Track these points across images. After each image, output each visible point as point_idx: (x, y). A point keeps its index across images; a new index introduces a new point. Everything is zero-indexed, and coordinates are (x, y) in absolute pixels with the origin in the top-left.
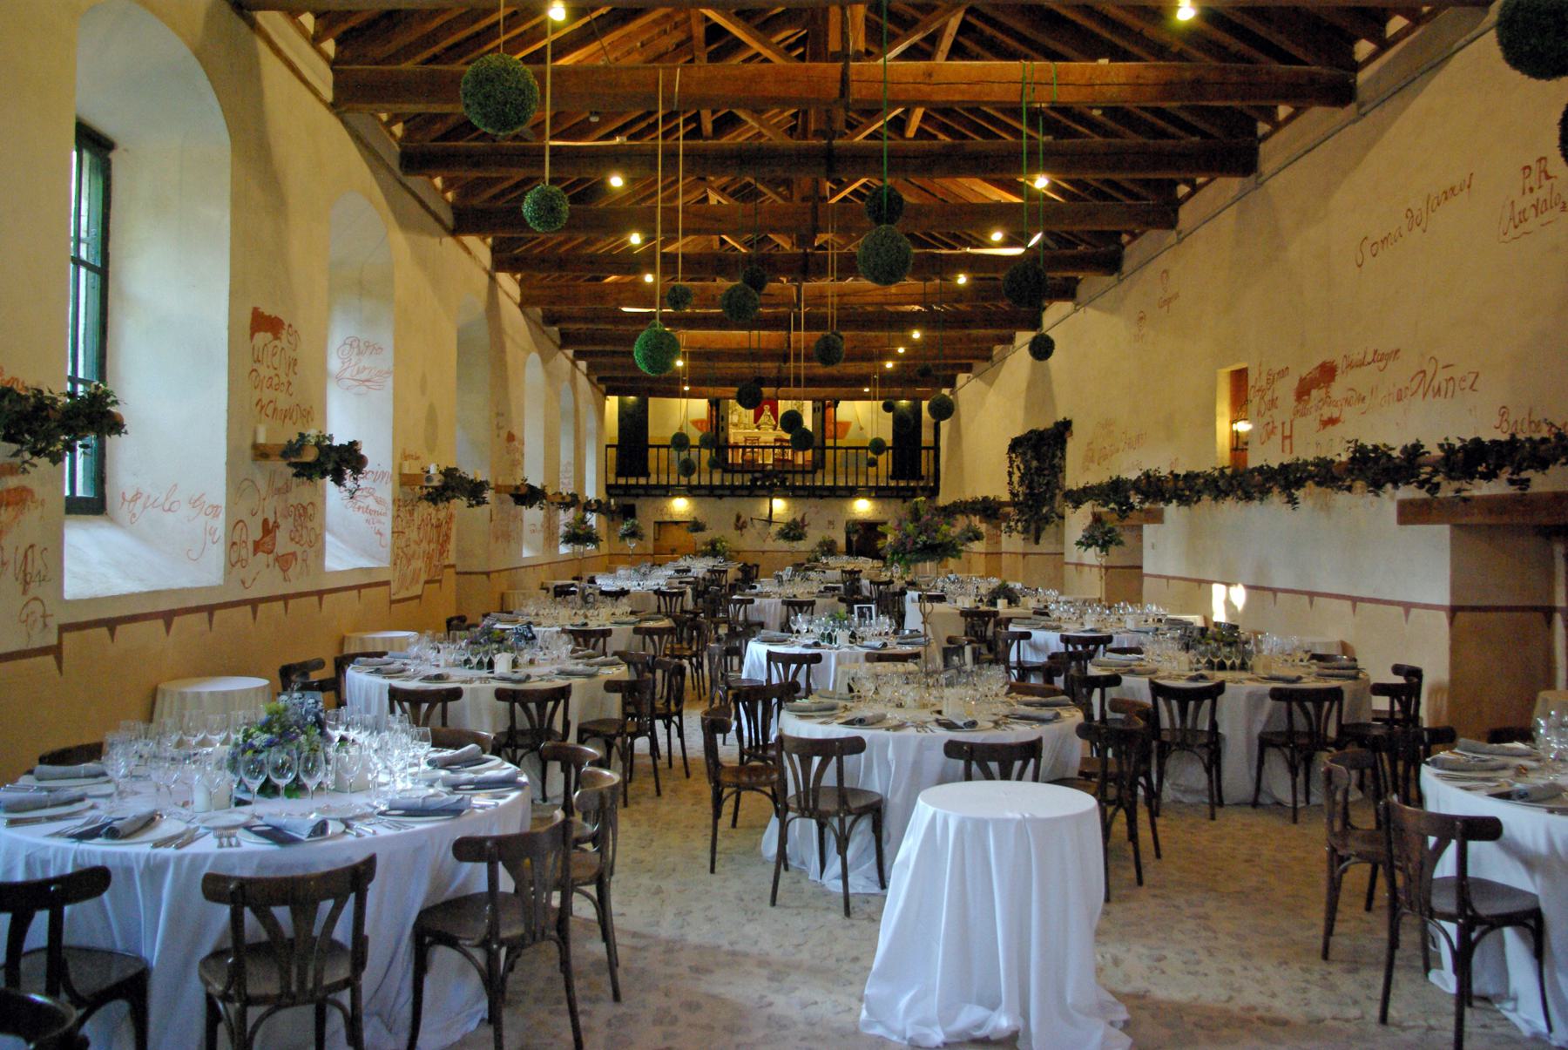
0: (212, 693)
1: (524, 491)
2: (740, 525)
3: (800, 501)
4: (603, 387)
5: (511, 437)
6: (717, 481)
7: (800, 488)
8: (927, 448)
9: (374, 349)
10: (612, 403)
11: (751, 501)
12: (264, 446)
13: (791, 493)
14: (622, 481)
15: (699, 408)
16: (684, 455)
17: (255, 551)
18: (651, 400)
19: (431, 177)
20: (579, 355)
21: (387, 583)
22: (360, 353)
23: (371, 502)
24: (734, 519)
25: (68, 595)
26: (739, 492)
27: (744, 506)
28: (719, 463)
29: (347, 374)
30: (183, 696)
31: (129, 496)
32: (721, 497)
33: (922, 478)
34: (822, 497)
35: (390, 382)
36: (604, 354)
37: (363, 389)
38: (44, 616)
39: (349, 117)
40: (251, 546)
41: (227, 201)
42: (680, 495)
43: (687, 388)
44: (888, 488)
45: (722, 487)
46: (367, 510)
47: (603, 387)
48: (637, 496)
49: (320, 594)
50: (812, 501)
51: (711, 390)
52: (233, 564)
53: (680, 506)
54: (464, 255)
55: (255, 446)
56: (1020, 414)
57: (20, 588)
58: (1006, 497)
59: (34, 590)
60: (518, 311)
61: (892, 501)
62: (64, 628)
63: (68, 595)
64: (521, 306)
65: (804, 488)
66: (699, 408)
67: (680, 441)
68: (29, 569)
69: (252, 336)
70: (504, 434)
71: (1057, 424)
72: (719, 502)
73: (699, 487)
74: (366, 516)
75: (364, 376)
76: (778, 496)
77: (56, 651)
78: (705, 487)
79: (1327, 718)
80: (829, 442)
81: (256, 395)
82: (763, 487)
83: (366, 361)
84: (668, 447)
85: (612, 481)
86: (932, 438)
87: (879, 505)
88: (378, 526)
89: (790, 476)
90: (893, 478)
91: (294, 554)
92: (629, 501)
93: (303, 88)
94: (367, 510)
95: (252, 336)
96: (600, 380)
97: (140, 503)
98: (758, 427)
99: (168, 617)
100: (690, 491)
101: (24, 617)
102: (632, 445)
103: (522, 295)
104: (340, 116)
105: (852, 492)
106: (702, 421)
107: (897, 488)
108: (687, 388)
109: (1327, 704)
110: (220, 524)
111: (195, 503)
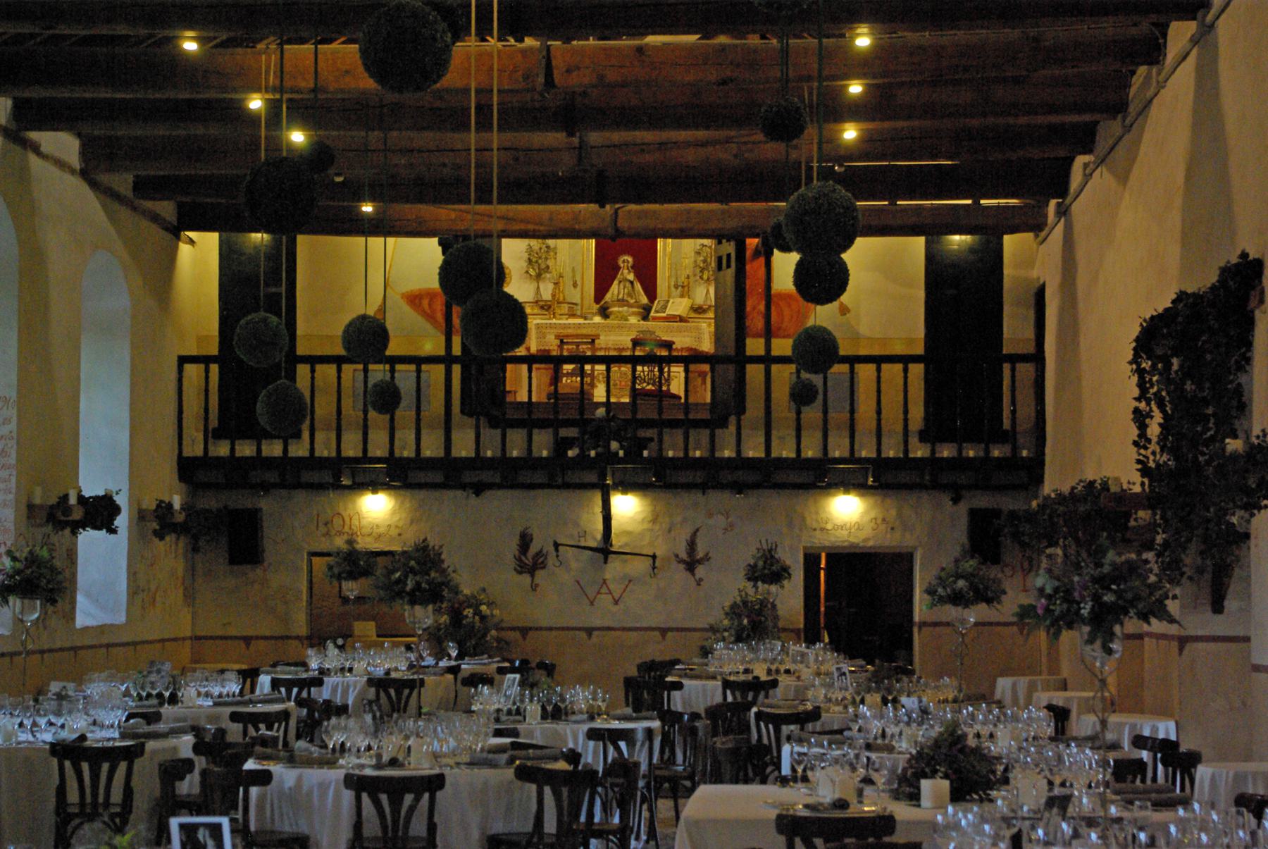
2: (530, 562)
3: (688, 498)
4: (167, 209)
6: (463, 447)
7: (675, 464)
8: (1014, 359)
10: (200, 255)
13: (654, 477)
14: (222, 449)
15: (418, 259)
16: (378, 372)
26: (525, 477)
27: (542, 512)
28: (484, 398)
33: (1008, 437)
34: (739, 488)
44: (905, 463)
45: (477, 462)
47: (167, 209)
48: (266, 488)
50: (721, 499)
51: (447, 214)
56: (1173, 253)
58: (1134, 482)
65: (686, 463)
66: (418, 259)
67: (367, 338)
71: (1226, 271)
72: (473, 500)
78: (431, 464)
80: (755, 346)
82: (582, 462)
84: (338, 361)
85: (194, 448)
86: (1030, 333)
87: (892, 506)
92: (241, 500)
96: (145, 188)
98: (604, 312)
100: (397, 474)
102: (254, 359)
105: (822, 476)
107: (933, 463)
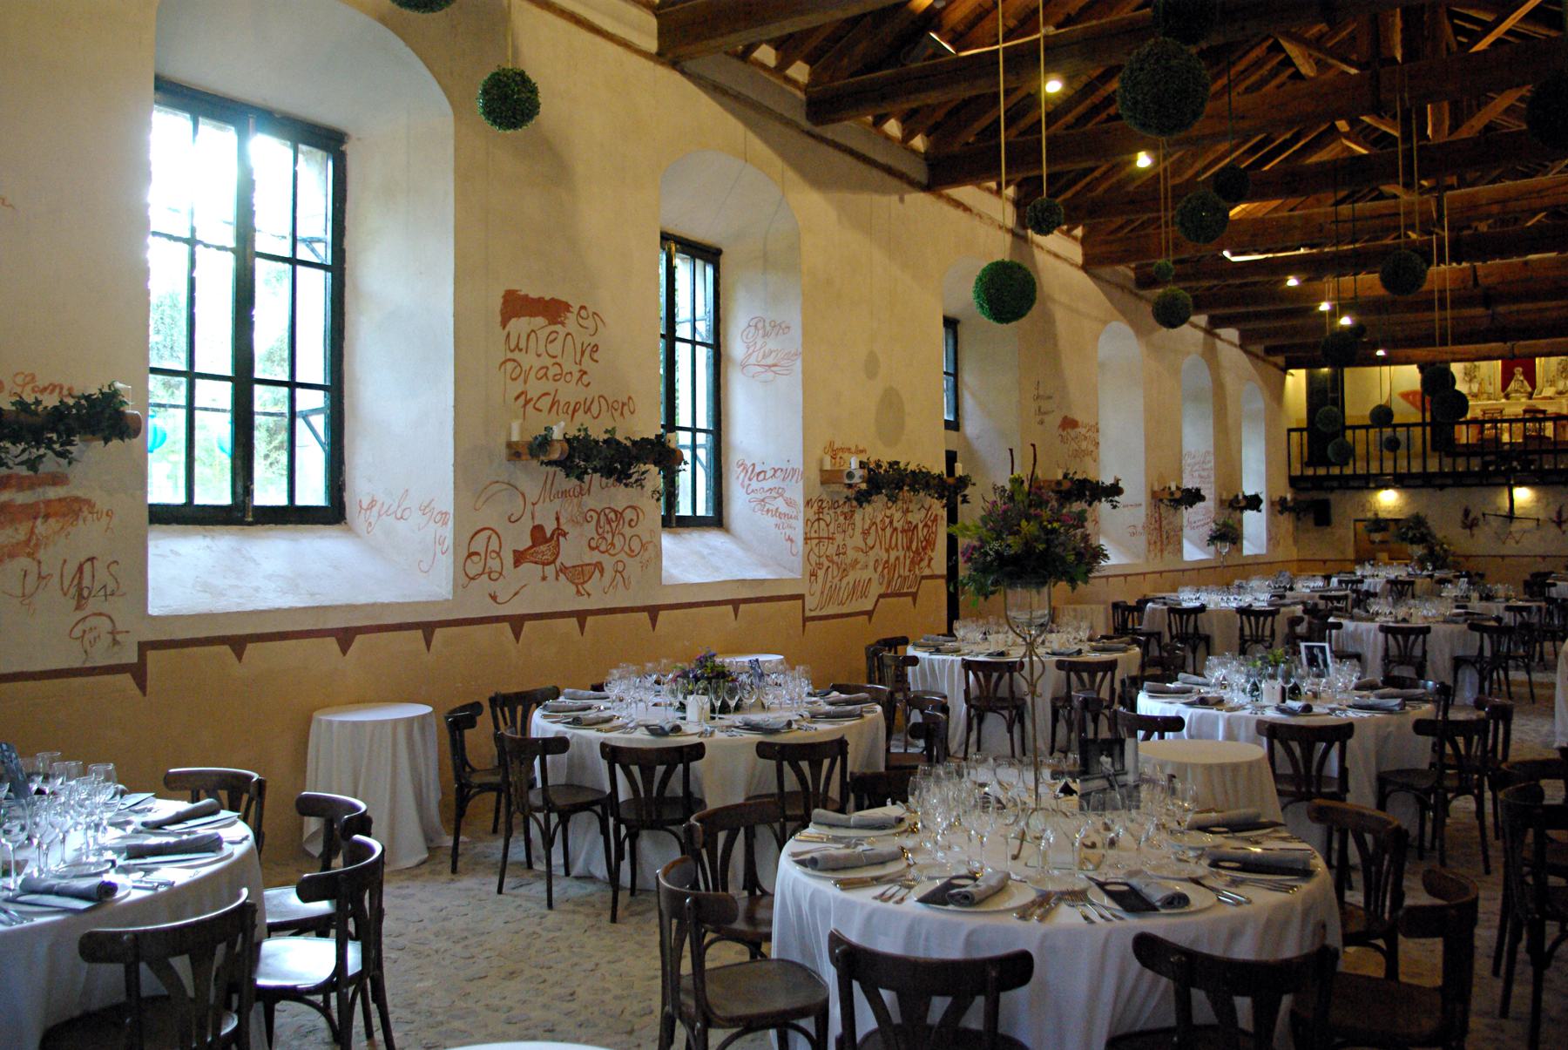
0: (342, 723)
1: (1066, 485)
2: (1469, 523)
4: (1280, 360)
5: (1069, 423)
6: (1433, 467)
9: (779, 328)
10: (1296, 381)
11: (1485, 491)
12: (517, 443)
15: (1408, 376)
16: (1388, 431)
17: (517, 563)
18: (1348, 372)
19: (880, 120)
20: (1216, 322)
21: (801, 597)
22: (765, 335)
23: (780, 503)
24: (1460, 515)
25: (153, 610)
27: (1475, 499)
28: (1442, 441)
29: (752, 360)
30: (320, 721)
31: (365, 506)
32: (1442, 487)
35: (798, 365)
36: (1258, 316)
37: (770, 375)
38: (113, 633)
39: (689, 65)
40: (509, 559)
41: (451, 177)
42: (1386, 487)
43: (1380, 353)
45: (1441, 474)
46: (777, 513)
48: (1332, 489)
49: (653, 611)
52: (465, 578)
53: (1388, 500)
54: (959, 213)
55: (509, 445)
57: (73, 603)
59: (92, 605)
60: (1081, 276)
61: (1424, 491)
62: (144, 647)
63: (153, 610)
64: (1086, 267)
66: (1408, 376)
67: (1382, 415)
68: (86, 582)
69: (504, 324)
70: (1054, 420)
73: (1410, 475)
74: (776, 520)
75: (770, 361)
76: (1521, 484)
77: (138, 672)
79: (828, 778)
81: (518, 387)
82: (1497, 472)
83: (772, 344)
84: (1367, 427)
85: (1296, 471)
88: (788, 532)
89: (1551, 458)
90: (1308, 464)
91: (599, 566)
93: (598, 40)
94: (777, 513)
95: (504, 324)
96: (1270, 351)
97: (375, 510)
98: (1507, 397)
99: (345, 637)
100: (1399, 481)
101: (77, 632)
103: (1085, 255)
104: (675, 65)
106: (1414, 393)
108: (1380, 353)
109: (826, 762)
110: (448, 532)
111: (425, 509)
